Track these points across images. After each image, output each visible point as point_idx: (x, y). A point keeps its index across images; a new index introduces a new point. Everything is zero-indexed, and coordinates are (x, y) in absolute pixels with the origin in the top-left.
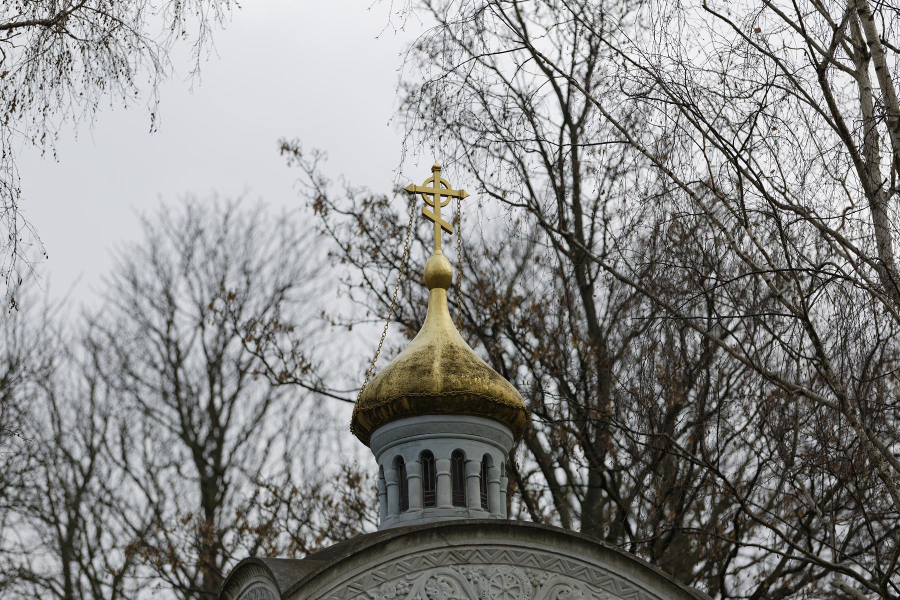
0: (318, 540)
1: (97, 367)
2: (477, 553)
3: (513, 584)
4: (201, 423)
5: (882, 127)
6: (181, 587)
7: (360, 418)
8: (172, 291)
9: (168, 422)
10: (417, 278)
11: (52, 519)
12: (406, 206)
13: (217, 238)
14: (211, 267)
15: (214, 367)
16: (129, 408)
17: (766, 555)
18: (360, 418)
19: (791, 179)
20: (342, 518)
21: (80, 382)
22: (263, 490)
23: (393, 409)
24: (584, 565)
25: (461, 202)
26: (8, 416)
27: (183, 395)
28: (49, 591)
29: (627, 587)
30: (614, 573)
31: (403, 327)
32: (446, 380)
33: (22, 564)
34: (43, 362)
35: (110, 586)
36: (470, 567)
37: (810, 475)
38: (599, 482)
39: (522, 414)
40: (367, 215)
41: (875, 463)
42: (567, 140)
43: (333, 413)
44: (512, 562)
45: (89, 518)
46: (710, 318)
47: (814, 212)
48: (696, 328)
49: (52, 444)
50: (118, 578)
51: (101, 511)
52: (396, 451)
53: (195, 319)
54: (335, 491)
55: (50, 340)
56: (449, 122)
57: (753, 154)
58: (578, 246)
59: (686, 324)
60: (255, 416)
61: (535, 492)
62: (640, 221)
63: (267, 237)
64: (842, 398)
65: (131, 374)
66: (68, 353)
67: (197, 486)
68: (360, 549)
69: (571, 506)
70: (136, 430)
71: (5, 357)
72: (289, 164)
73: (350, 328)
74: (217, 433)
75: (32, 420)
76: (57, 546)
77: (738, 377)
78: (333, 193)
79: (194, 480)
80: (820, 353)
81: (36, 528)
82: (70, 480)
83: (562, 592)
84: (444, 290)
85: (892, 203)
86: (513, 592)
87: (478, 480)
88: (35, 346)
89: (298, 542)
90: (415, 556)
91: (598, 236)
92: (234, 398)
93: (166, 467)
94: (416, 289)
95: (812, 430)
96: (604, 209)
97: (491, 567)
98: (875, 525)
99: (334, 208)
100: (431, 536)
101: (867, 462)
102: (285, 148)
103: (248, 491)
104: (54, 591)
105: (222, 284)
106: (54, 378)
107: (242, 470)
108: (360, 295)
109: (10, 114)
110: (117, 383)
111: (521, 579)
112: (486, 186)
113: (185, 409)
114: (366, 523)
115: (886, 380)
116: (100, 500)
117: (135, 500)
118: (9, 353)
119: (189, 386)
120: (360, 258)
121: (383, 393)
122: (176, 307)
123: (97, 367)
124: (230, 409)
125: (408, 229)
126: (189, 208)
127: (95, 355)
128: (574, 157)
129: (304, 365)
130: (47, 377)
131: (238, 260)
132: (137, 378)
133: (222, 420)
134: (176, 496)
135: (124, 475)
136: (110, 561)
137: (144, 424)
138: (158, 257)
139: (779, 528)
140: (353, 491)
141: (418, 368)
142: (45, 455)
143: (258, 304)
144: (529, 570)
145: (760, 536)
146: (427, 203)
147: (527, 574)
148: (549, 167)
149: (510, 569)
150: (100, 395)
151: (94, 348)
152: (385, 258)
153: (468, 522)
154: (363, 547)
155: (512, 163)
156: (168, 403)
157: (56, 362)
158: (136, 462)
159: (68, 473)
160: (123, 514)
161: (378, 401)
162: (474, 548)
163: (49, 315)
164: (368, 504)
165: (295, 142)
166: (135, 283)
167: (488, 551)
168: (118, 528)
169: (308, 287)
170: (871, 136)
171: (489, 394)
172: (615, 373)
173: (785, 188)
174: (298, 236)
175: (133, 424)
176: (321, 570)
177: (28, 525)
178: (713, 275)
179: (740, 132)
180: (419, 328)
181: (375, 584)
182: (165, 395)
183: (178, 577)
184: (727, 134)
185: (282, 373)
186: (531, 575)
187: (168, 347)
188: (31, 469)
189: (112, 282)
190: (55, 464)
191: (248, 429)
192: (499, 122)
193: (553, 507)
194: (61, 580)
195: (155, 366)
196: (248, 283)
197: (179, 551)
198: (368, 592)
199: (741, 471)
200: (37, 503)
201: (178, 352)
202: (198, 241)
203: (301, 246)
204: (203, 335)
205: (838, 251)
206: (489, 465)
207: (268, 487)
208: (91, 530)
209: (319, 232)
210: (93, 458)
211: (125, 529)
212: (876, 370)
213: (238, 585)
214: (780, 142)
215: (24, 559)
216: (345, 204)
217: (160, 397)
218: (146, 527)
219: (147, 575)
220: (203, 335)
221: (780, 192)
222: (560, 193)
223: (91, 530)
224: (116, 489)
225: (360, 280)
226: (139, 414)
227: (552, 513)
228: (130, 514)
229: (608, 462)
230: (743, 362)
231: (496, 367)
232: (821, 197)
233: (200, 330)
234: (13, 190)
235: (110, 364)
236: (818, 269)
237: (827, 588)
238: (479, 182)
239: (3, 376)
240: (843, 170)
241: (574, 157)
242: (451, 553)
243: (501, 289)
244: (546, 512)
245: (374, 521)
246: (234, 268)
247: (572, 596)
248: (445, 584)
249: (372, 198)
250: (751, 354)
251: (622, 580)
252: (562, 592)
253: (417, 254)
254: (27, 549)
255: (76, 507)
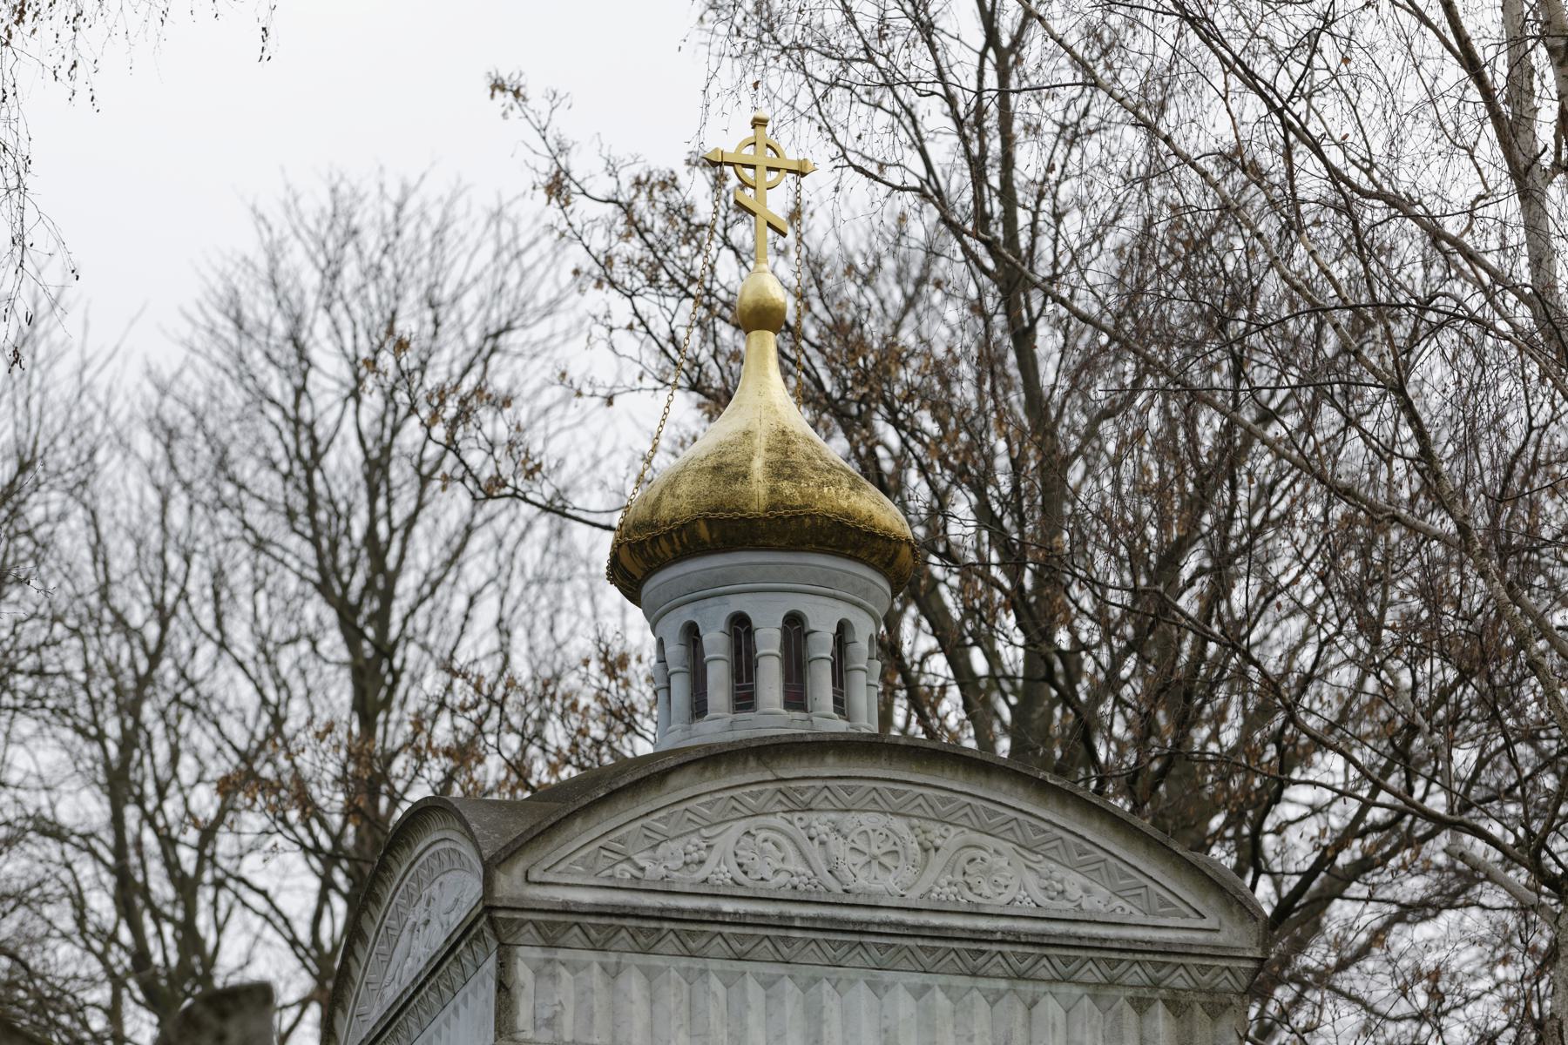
0: (554, 769)
1: (173, 467)
2: (826, 792)
3: (888, 847)
4: (353, 565)
5: (1540, 56)
6: (317, 849)
7: (624, 555)
8: (304, 335)
9: (296, 565)
10: (726, 312)
11: (92, 731)
12: (708, 189)
13: (383, 243)
14: (372, 292)
15: (376, 469)
16: (228, 539)
17: (1334, 800)
18: (624, 555)
19: (1378, 148)
20: (597, 731)
21: (141, 491)
22: (458, 682)
23: (681, 541)
24: (1012, 814)
25: (803, 180)
26: (16, 551)
27: (322, 516)
28: (86, 855)
29: (1086, 853)
30: (1063, 828)
31: (702, 399)
32: (773, 491)
33: (38, 809)
34: (78, 457)
35: (192, 847)
36: (813, 816)
37: (1412, 663)
38: (1042, 673)
39: (906, 550)
40: (641, 204)
41: (1522, 643)
42: (991, 80)
43: (583, 550)
44: (887, 808)
45: (158, 730)
46: (1236, 391)
47: (1420, 203)
48: (1211, 403)
49: (94, 600)
50: (208, 834)
51: (179, 718)
52: (686, 614)
53: (343, 384)
54: (585, 685)
55: (91, 418)
56: (786, 42)
57: (1314, 101)
58: (1009, 261)
59: (1198, 397)
60: (447, 555)
61: (931, 687)
62: (1117, 218)
63: (470, 242)
64: (1463, 529)
65: (231, 479)
66: (123, 444)
67: (345, 674)
68: (621, 784)
69: (997, 715)
70: (240, 577)
71: (12, 447)
72: (504, 115)
73: (610, 401)
74: (380, 583)
75: (60, 559)
76: (101, 778)
77: (1284, 492)
78: (581, 166)
79: (340, 664)
80: (1426, 453)
81: (64, 746)
82: (124, 663)
83: (973, 860)
84: (771, 334)
85: (1553, 191)
86: (887, 861)
87: (828, 665)
88: (64, 429)
89: (518, 768)
90: (718, 795)
91: (1045, 243)
92: (412, 520)
93: (294, 641)
94: (726, 332)
95: (1414, 585)
96: (1055, 196)
97: (849, 816)
98: (1522, 749)
99: (584, 193)
100: (746, 761)
101: (1509, 641)
102: (498, 86)
103: (433, 683)
104: (94, 854)
105: (391, 322)
106: (97, 485)
107: (424, 647)
108: (628, 343)
109: (14, 29)
110: (208, 495)
111: (902, 838)
112: (849, 154)
113: (324, 543)
114: (638, 741)
115: (1544, 497)
116: (177, 698)
117: (238, 699)
118: (17, 440)
119: (331, 501)
120: (628, 277)
121: (665, 513)
122: (310, 365)
123: (173, 467)
124: (404, 540)
125: (712, 229)
126: (334, 190)
127: (168, 447)
128: (1004, 106)
129: (530, 465)
130: (84, 483)
131: (419, 281)
132: (242, 487)
133: (391, 562)
134: (309, 692)
135: (219, 654)
136: (194, 805)
137: (254, 568)
138: (279, 278)
139: (1356, 754)
140: (613, 684)
141: (725, 470)
142: (79, 617)
143: (452, 361)
144: (915, 822)
145: (1322, 766)
146: (744, 185)
147: (912, 828)
148: (959, 123)
149: (883, 819)
150: (177, 517)
151: (170, 435)
152: (673, 280)
153: (809, 738)
154: (628, 779)
155: (893, 113)
156: (294, 530)
157: (100, 457)
158: (240, 633)
159: (118, 649)
160: (217, 724)
161: (655, 527)
162: (819, 784)
163: (87, 375)
164: (643, 707)
165: (515, 78)
166: (239, 322)
167: (845, 788)
168: (207, 747)
169: (540, 331)
170: (1521, 69)
171: (848, 516)
172: (1071, 483)
173: (1370, 162)
174: (522, 243)
175: (235, 567)
176: (553, 819)
177: (51, 742)
178: (1243, 314)
179: (1291, 61)
180: (730, 398)
181: (647, 844)
182: (291, 515)
183: (311, 833)
184: (1265, 68)
185: (491, 477)
186: (918, 831)
187: (296, 434)
188: (56, 643)
189: (200, 319)
190: (98, 635)
191: (435, 576)
192: (872, 44)
193: (963, 715)
194: (109, 837)
195: (274, 466)
196: (437, 323)
197: (315, 791)
198: (636, 858)
199: (1293, 652)
200: (65, 702)
201: (314, 441)
202: (350, 249)
203: (527, 260)
204: (357, 412)
205: (1461, 272)
206: (848, 639)
207: (465, 676)
208: (161, 750)
209: (556, 234)
210: (164, 626)
211: (219, 749)
212: (1525, 481)
213: (409, 845)
214: (1361, 81)
215: (43, 799)
216: (602, 186)
217: (282, 519)
218: (255, 745)
219: (258, 830)
220: (357, 412)
221: (1362, 169)
222: (977, 166)
223: (161, 750)
224: (202, 680)
225: (629, 318)
226: (245, 549)
227: (961, 723)
228: (229, 724)
229: (1063, 638)
230: (1295, 465)
231: (864, 471)
232: (1429, 180)
233: (351, 404)
234: (19, 159)
235: (195, 460)
236: (1424, 306)
237: (1441, 859)
238: (836, 148)
239: (6, 481)
240: (1468, 128)
241: (1004, 106)
242: (780, 791)
243: (874, 330)
244: (952, 722)
245: (651, 737)
246: (412, 296)
247: (990, 868)
248: (769, 846)
249: (650, 174)
250: (1308, 451)
251: (1078, 841)
252: (973, 860)
253: (727, 271)
254: (47, 783)
255: (136, 712)
